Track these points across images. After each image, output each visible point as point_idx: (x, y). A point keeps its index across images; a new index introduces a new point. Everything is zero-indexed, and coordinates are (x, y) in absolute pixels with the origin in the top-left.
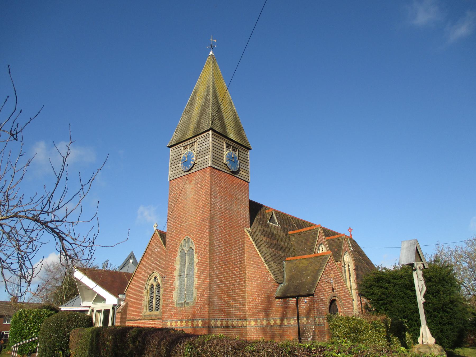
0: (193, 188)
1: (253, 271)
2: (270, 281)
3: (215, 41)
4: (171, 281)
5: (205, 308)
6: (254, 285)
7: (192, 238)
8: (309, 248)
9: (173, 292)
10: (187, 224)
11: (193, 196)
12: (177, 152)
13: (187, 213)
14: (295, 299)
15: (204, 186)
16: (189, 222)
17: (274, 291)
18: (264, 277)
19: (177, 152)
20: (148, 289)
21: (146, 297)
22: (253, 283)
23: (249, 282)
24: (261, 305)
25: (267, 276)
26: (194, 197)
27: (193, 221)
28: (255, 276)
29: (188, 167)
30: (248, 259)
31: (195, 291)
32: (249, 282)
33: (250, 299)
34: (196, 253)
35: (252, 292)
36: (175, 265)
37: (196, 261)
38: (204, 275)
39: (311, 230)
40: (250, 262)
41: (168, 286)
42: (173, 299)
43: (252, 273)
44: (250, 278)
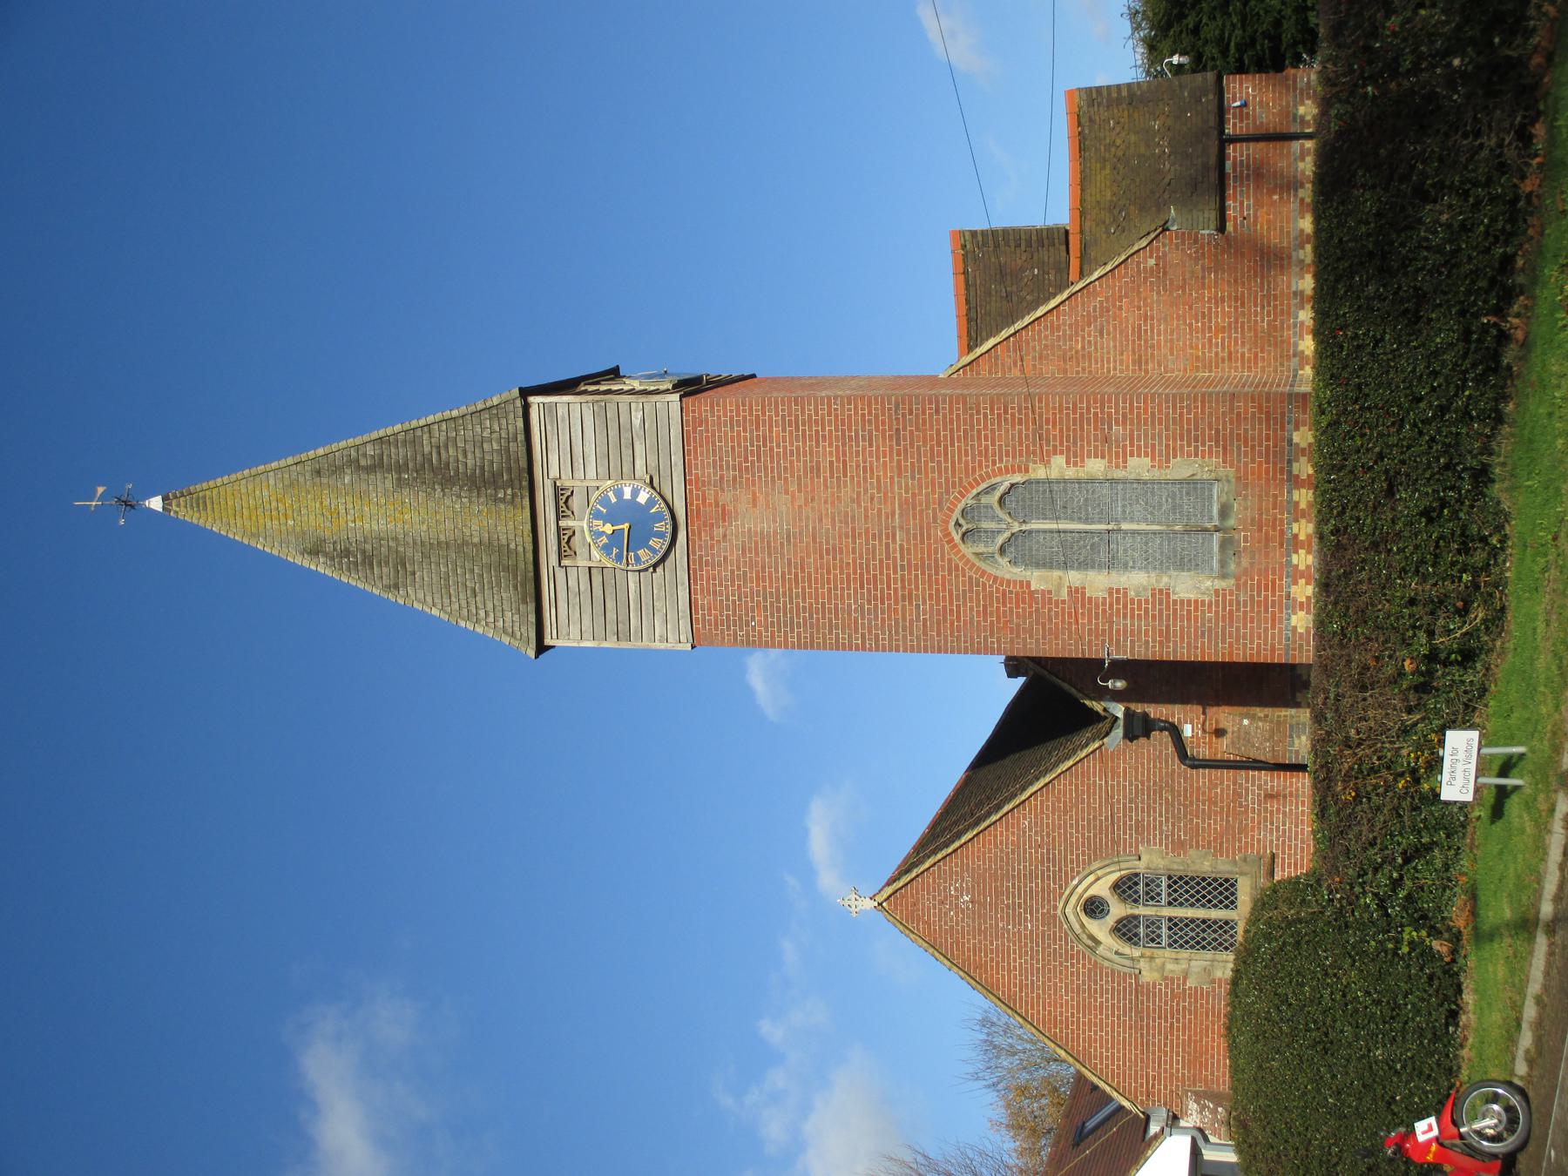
0: (754, 499)
1: (1115, 337)
2: (1158, 258)
3: (100, 490)
4: (1125, 617)
5: (1246, 412)
6: (1165, 336)
7: (963, 496)
8: (1036, 255)
9: (1175, 602)
10: (901, 528)
11: (787, 492)
12: (574, 601)
13: (853, 530)
14: (1230, 150)
15: (758, 429)
16: (893, 514)
17: (1196, 241)
18: (1139, 287)
19: (574, 601)
20: (1136, 952)
21: (1169, 966)
22: (1159, 342)
23: (1153, 362)
24: (1243, 305)
25: (1139, 272)
26: (793, 488)
27: (892, 493)
28: (1133, 330)
29: (661, 535)
30: (1065, 361)
31: (1181, 468)
32: (1153, 362)
33: (1217, 354)
34: (1027, 471)
35: (1191, 347)
36: (1064, 595)
37: (1058, 466)
38: (1117, 423)
39: (966, 266)
40: (1077, 352)
41: (1147, 631)
42: (1200, 597)
43: (1121, 343)
44: (1140, 356)
